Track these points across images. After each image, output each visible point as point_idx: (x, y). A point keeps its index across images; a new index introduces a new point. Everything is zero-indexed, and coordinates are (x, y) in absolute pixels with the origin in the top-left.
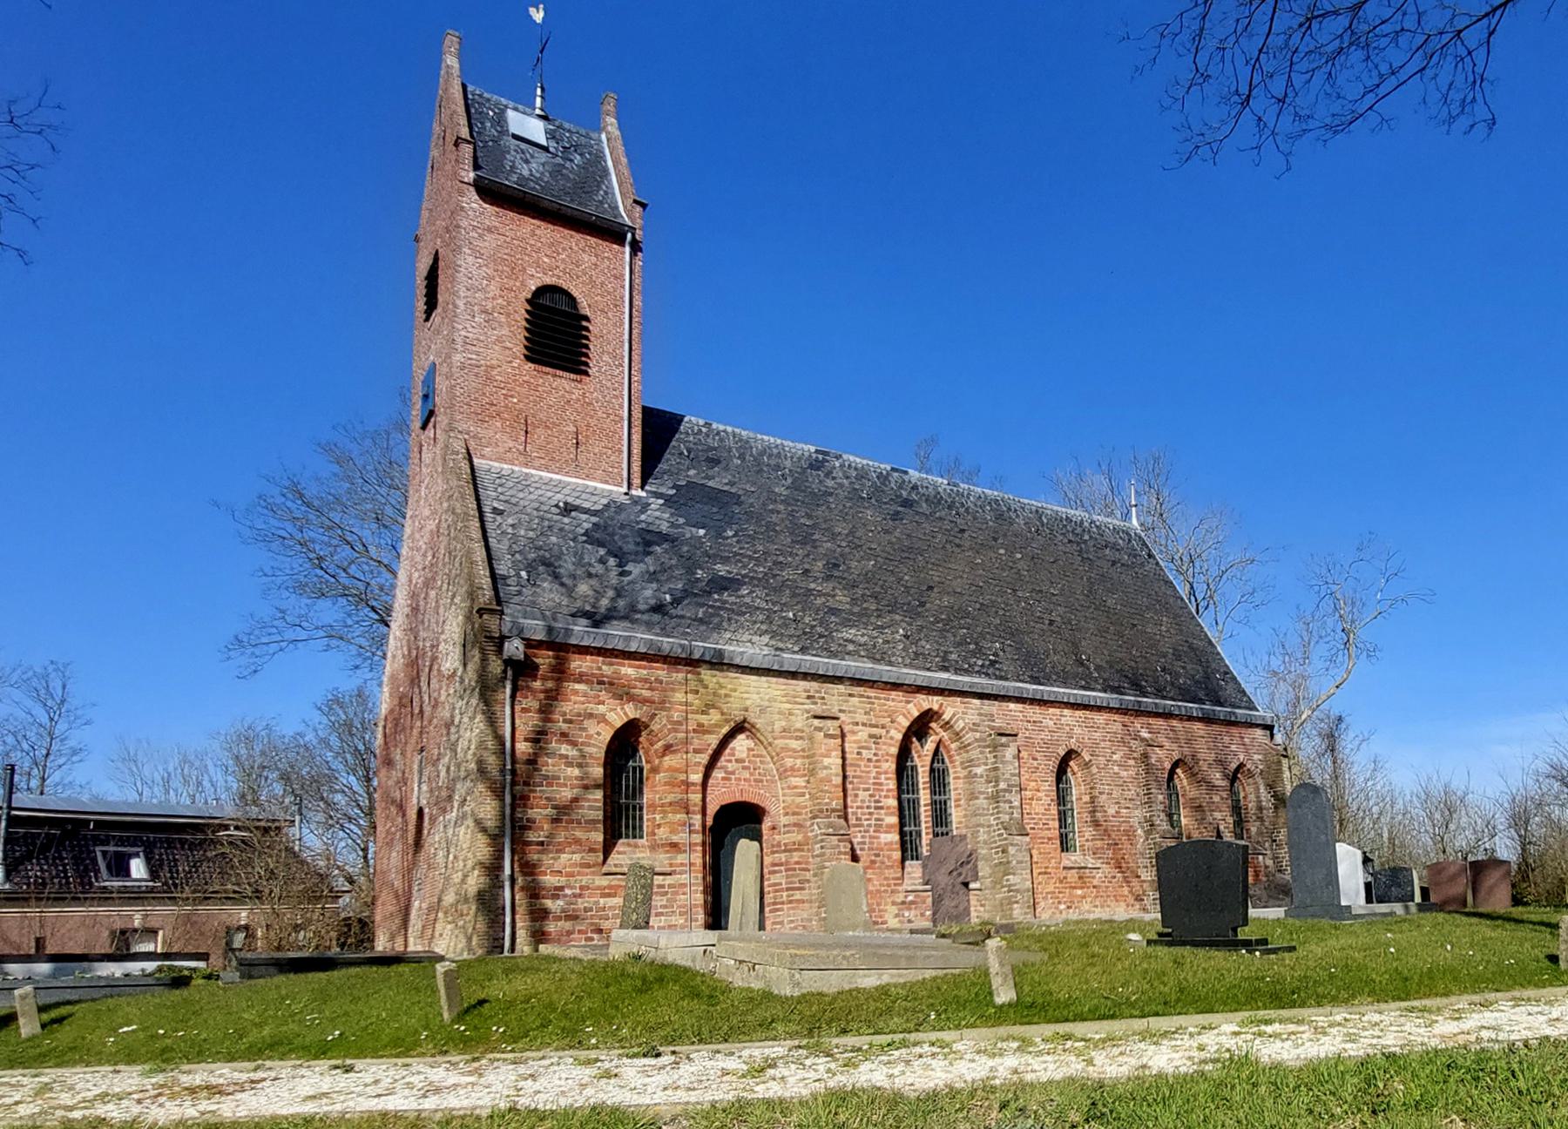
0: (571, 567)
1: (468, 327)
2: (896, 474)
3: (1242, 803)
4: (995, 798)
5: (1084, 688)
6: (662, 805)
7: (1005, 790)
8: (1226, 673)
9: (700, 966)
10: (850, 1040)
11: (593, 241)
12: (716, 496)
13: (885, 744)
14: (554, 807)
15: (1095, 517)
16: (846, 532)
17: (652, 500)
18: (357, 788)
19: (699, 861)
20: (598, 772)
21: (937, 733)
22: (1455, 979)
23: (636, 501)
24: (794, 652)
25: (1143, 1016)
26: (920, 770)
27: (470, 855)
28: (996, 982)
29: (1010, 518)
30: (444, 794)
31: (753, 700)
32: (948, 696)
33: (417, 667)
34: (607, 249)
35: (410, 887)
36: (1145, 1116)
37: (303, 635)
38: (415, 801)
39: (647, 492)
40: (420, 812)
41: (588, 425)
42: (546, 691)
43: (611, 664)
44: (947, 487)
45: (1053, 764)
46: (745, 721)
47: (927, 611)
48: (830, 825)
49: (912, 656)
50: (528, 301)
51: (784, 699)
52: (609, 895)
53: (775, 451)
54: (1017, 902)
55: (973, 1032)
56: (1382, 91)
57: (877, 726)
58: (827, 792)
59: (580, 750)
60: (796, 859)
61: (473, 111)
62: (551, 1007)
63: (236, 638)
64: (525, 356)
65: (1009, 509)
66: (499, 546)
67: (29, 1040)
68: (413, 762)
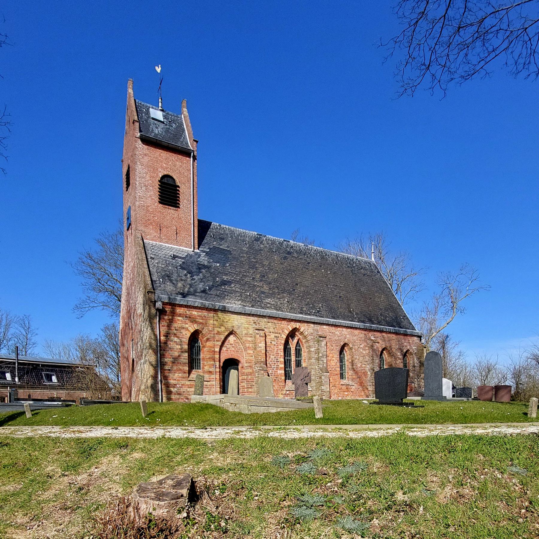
0: (176, 277)
1: (140, 192)
2: (285, 242)
3: (407, 364)
4: (318, 359)
5: (350, 321)
6: (207, 359)
7: (321, 357)
8: (405, 316)
9: (219, 404)
10: (267, 427)
11: (180, 157)
12: (222, 252)
13: (280, 339)
14: (173, 358)
15: (358, 257)
16: (267, 264)
17: (201, 253)
18: (114, 356)
19: (218, 378)
20: (186, 347)
21: (298, 336)
22: (485, 418)
23: (196, 254)
24: (250, 307)
25: (367, 424)
26: (292, 349)
27: (148, 373)
28: (316, 411)
29: (326, 258)
30: (140, 354)
31: (236, 323)
32: (302, 323)
33: (130, 313)
34: (185, 159)
35: (131, 384)
36: (366, 448)
37: (96, 305)
38: (131, 357)
39: (200, 250)
40: (133, 360)
41: (180, 226)
42: (169, 320)
43: (189, 311)
44: (304, 247)
45: (339, 348)
46: (233, 330)
47: (296, 293)
48: (261, 367)
49: (290, 308)
50: (159, 181)
51: (246, 323)
52: (190, 387)
53: (243, 235)
54: (324, 396)
55: (308, 426)
56: (488, 59)
57: (277, 333)
58: (260, 355)
59: (180, 340)
60: (250, 378)
61: (138, 109)
62: (174, 414)
63: (76, 305)
64: (159, 202)
65: (326, 255)
66: (153, 270)
67: (29, 419)
68: (130, 344)
